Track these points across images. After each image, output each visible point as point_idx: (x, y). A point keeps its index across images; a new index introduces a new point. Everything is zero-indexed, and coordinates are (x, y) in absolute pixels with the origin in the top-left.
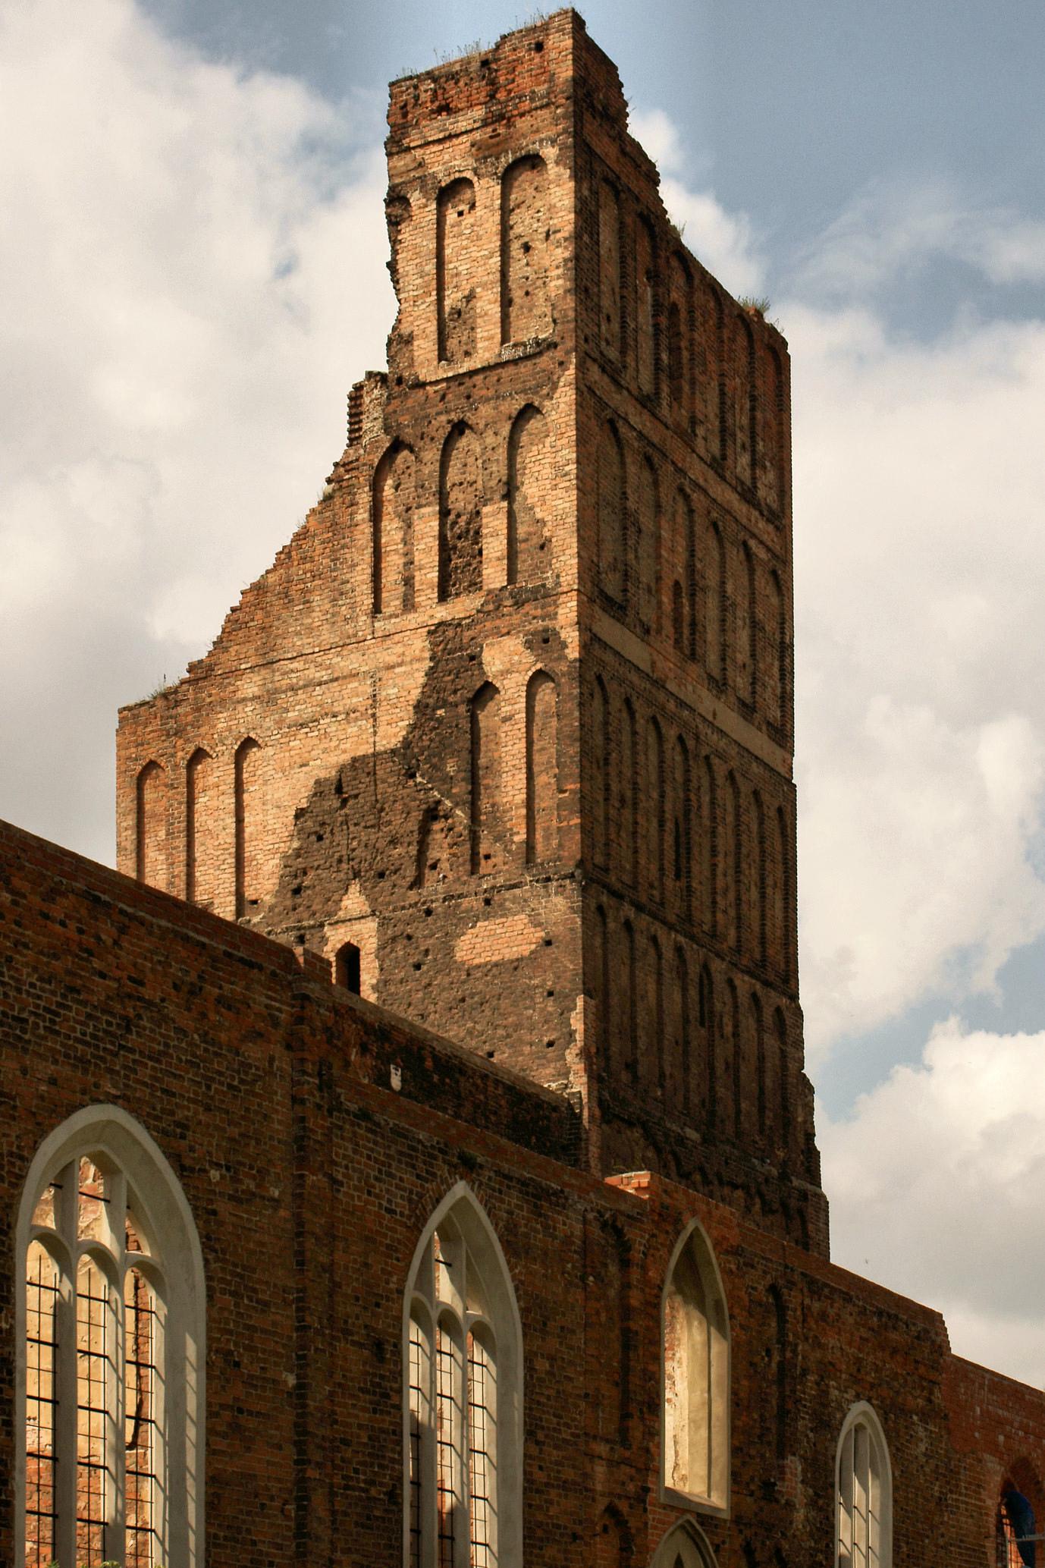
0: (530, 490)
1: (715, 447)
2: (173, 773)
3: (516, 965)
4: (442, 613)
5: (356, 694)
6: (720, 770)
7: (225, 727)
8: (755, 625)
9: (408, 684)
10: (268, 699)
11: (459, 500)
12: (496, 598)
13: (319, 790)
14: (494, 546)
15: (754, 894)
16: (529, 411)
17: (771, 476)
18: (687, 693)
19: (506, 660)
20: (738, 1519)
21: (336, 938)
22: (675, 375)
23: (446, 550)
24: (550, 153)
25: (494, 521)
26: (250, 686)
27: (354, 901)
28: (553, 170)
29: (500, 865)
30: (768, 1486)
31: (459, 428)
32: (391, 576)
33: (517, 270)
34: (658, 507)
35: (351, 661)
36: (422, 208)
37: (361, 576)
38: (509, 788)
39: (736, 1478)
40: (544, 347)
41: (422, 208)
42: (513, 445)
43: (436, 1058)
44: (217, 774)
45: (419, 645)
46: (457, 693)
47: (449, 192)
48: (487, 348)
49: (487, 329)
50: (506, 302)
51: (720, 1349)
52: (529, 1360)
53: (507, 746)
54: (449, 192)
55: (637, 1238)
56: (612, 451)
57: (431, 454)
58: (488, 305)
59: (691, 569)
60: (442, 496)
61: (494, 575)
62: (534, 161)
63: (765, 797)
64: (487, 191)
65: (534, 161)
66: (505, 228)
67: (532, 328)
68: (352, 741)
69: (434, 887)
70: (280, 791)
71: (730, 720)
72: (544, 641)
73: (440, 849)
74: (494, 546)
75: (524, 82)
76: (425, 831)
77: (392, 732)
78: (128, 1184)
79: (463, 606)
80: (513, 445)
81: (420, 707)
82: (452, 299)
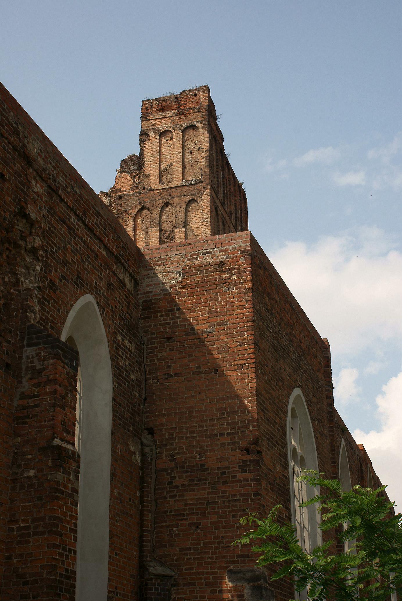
11: (166, 227)
24: (200, 125)
28: (201, 130)
31: (167, 204)
40: (197, 182)
42: (186, 211)
50: (184, 168)
57: (156, 212)
60: (160, 225)
64: (177, 135)
65: (194, 127)
66: (184, 146)
80: (186, 211)
82: (164, 165)
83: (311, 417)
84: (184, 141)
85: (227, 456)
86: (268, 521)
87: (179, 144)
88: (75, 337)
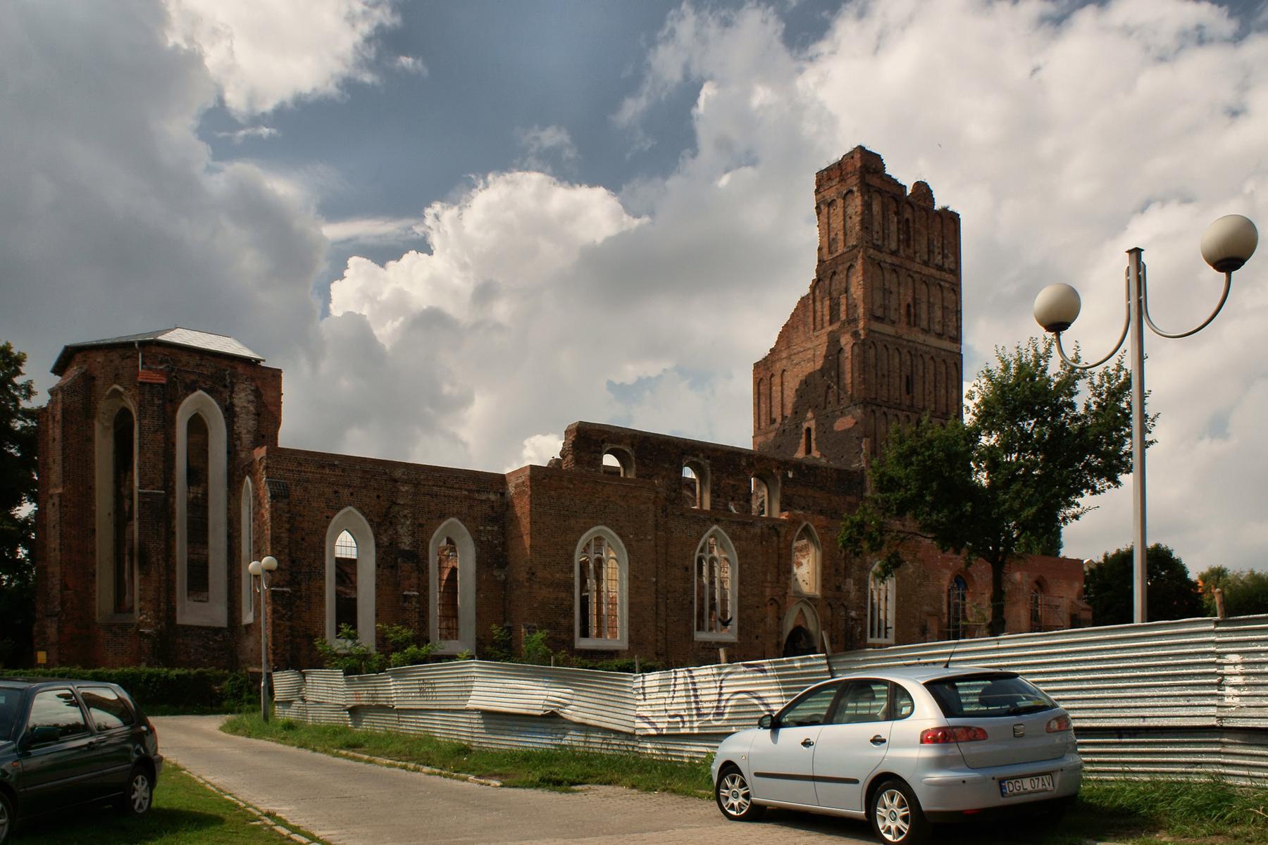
0: (852, 290)
1: (926, 257)
2: (766, 382)
3: (849, 430)
4: (830, 329)
5: (810, 354)
6: (927, 357)
7: (778, 366)
8: (944, 308)
9: (822, 350)
10: (789, 357)
11: (835, 294)
12: (843, 323)
13: (801, 384)
14: (843, 308)
15: (943, 391)
16: (851, 266)
17: (952, 259)
18: (912, 337)
19: (846, 341)
20: (824, 597)
21: (805, 425)
22: (908, 240)
23: (831, 308)
24: (855, 189)
25: (843, 301)
26: (784, 355)
27: (810, 415)
28: (856, 194)
29: (845, 402)
30: (838, 588)
31: (834, 273)
32: (818, 319)
33: (848, 225)
34: (899, 284)
35: (809, 345)
36: (824, 210)
37: (811, 319)
38: (848, 378)
39: (823, 586)
40: (854, 247)
41: (824, 210)
42: (847, 276)
43: (807, 466)
44: (777, 380)
45: (825, 338)
46: (834, 350)
47: (830, 204)
48: (841, 249)
49: (841, 244)
50: (845, 234)
51: (819, 554)
52: (740, 566)
53: (847, 367)
54: (830, 204)
55: (783, 531)
56: (879, 272)
57: (827, 282)
58: (841, 237)
59: (914, 299)
60: (830, 293)
61: (843, 317)
62: (850, 192)
63: (948, 361)
64: (840, 202)
65: (850, 192)
66: (845, 212)
67: (853, 242)
68: (809, 368)
69: (829, 409)
70: (792, 384)
71: (933, 341)
72: (855, 334)
73: (831, 398)
74: (843, 308)
75: (849, 169)
76: (827, 393)
77: (819, 364)
78: (763, 502)
79: (835, 326)
80: (847, 276)
81: (826, 357)
82: (832, 235)
83: (171, 533)
84: (845, 208)
85: (700, 636)
86: (878, 495)
87: (841, 214)
88: (28, 359)
